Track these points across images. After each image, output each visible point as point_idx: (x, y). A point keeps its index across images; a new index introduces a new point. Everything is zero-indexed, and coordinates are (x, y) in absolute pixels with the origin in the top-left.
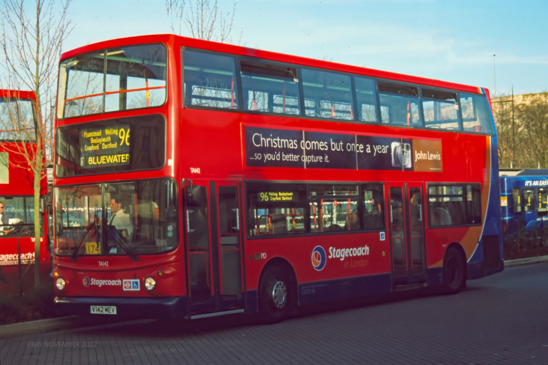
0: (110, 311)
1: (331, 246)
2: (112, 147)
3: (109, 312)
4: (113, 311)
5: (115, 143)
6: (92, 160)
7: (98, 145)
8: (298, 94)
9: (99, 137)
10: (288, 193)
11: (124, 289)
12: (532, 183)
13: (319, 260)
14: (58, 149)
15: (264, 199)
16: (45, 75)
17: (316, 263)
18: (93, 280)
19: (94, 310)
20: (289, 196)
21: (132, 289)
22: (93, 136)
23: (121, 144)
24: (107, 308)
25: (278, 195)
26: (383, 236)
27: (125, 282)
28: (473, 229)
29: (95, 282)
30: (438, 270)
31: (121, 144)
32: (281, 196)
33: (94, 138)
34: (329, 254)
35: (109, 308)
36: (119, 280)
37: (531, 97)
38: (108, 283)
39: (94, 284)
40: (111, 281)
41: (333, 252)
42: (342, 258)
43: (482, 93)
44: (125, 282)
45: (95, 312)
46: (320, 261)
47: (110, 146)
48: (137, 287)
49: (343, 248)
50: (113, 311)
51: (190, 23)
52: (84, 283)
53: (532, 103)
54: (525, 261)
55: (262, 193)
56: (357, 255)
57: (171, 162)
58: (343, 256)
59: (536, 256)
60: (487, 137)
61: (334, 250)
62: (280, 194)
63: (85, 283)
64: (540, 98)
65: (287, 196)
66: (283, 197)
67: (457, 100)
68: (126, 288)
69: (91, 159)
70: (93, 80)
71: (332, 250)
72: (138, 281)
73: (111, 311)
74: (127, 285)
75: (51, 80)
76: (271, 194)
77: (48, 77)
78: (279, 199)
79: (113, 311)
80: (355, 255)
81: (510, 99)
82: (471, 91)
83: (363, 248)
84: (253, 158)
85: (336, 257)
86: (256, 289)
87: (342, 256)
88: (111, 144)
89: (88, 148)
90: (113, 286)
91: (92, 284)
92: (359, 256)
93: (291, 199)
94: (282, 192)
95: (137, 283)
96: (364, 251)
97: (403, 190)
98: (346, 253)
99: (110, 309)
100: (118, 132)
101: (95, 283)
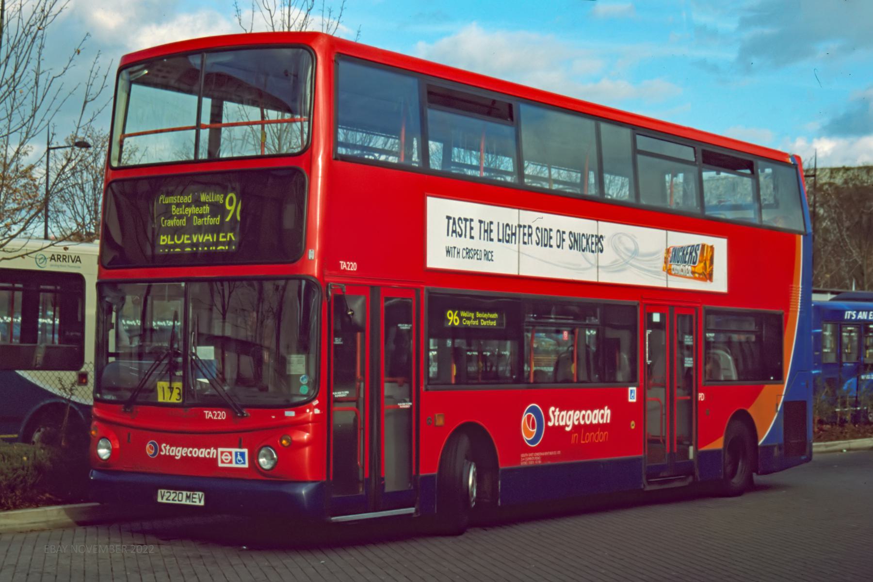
0: (194, 500)
1: (552, 405)
2: (211, 224)
3: (193, 502)
4: (200, 501)
5: (217, 217)
7: (185, 218)
8: (513, 151)
9: (188, 205)
10: (490, 313)
11: (220, 465)
12: (857, 315)
13: (533, 427)
15: (453, 323)
16: (9, 87)
17: (528, 433)
18: (165, 447)
19: (162, 498)
20: (492, 320)
21: (234, 465)
22: (175, 202)
23: (228, 219)
24: (190, 494)
25: (475, 316)
26: (633, 394)
27: (222, 453)
28: (768, 389)
29: (169, 450)
30: (717, 453)
31: (228, 219)
32: (479, 319)
33: (178, 205)
34: (548, 419)
35: (193, 494)
36: (212, 448)
37: (844, 173)
39: (167, 454)
40: (199, 449)
41: (554, 416)
42: (568, 426)
43: (792, 163)
44: (222, 453)
45: (164, 501)
46: (535, 430)
47: (207, 221)
48: (242, 461)
49: (571, 410)
50: (198, 499)
51: (269, 10)
52: (149, 451)
53: (846, 182)
54: (827, 446)
55: (450, 312)
56: (591, 423)
57: (312, 254)
58: (570, 423)
59: (845, 438)
60: (797, 236)
61: (557, 413)
62: (479, 315)
63: (149, 451)
64: (858, 175)
65: (489, 319)
66: (482, 320)
67: (753, 172)
68: (222, 462)
70: (93, 100)
71: (553, 412)
72: (246, 451)
73: (197, 500)
74: (226, 457)
75: (18, 94)
76: (463, 314)
77: (14, 90)
78: (476, 323)
79: (200, 501)
80: (588, 422)
81: (812, 172)
82: (776, 159)
83: (602, 411)
84: (214, 248)
85: (559, 424)
86: (436, 473)
87: (568, 423)
88: (210, 218)
89: (167, 222)
90: (202, 458)
91: (162, 453)
92: (595, 425)
93: (494, 323)
94: (481, 312)
95: (242, 454)
98: (576, 418)
99: (194, 496)
100: (224, 199)
101: (169, 452)
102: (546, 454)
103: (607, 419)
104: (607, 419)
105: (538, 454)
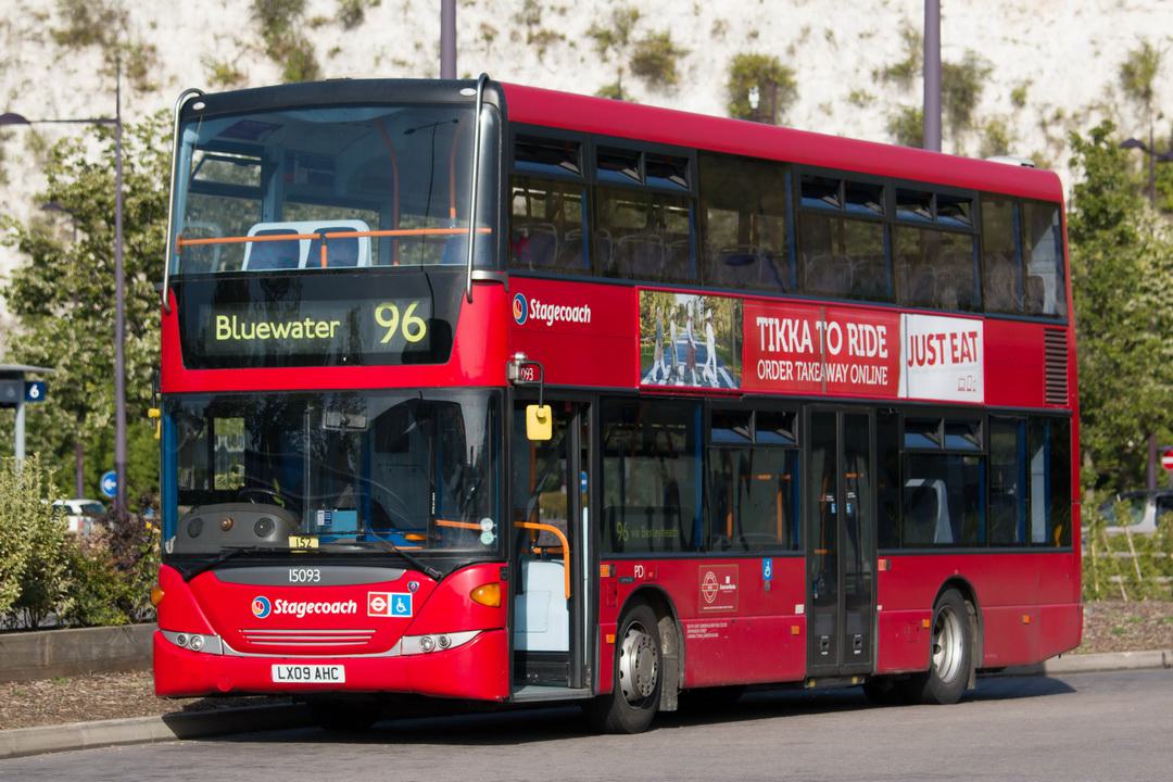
6: (231, 325)
14: (462, 250)
18: (280, 604)
38: (323, 609)
39: (285, 612)
58: (551, 318)
61: (538, 306)
69: (223, 322)
80: (569, 319)
83: (582, 310)
90: (326, 615)
96: (583, 315)
97: (1024, 321)
98: (556, 313)
100: (630, 535)
101: (287, 609)
102: (712, 625)
103: (587, 319)
104: (587, 319)
105: (703, 626)
